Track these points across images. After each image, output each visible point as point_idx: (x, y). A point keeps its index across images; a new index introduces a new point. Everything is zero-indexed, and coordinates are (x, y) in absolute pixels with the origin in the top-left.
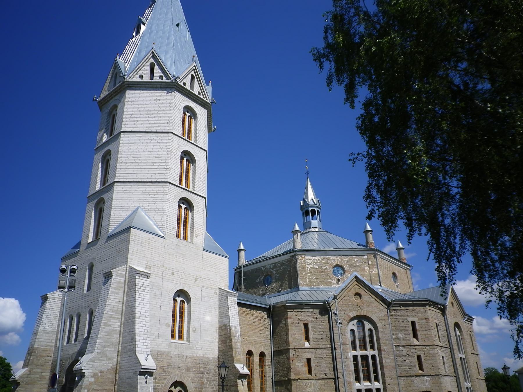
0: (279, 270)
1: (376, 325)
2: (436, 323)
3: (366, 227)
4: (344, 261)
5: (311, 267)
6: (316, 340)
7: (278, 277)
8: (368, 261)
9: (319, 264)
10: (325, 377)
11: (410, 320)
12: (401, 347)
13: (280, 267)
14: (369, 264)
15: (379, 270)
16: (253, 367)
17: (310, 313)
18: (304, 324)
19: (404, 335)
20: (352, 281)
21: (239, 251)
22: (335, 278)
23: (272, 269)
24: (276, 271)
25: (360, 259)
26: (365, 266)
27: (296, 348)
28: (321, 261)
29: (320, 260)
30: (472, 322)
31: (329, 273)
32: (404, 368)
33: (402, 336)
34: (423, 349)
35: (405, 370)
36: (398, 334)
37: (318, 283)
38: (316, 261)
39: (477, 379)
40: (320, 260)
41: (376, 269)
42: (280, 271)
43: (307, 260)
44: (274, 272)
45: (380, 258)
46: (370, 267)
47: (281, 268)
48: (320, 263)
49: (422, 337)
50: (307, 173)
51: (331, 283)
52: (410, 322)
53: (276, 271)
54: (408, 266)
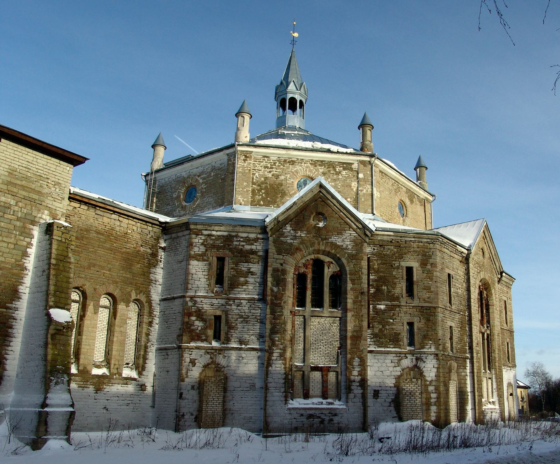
0: (208, 177)
2: (449, 275)
5: (259, 175)
7: (205, 188)
8: (358, 174)
14: (358, 178)
15: (375, 189)
16: (115, 322)
24: (203, 179)
26: (352, 181)
29: (277, 164)
31: (289, 187)
33: (387, 289)
38: (269, 166)
41: (369, 187)
42: (210, 178)
43: (254, 163)
44: (201, 181)
46: (360, 182)
47: (212, 175)
52: (405, 268)
53: (203, 179)
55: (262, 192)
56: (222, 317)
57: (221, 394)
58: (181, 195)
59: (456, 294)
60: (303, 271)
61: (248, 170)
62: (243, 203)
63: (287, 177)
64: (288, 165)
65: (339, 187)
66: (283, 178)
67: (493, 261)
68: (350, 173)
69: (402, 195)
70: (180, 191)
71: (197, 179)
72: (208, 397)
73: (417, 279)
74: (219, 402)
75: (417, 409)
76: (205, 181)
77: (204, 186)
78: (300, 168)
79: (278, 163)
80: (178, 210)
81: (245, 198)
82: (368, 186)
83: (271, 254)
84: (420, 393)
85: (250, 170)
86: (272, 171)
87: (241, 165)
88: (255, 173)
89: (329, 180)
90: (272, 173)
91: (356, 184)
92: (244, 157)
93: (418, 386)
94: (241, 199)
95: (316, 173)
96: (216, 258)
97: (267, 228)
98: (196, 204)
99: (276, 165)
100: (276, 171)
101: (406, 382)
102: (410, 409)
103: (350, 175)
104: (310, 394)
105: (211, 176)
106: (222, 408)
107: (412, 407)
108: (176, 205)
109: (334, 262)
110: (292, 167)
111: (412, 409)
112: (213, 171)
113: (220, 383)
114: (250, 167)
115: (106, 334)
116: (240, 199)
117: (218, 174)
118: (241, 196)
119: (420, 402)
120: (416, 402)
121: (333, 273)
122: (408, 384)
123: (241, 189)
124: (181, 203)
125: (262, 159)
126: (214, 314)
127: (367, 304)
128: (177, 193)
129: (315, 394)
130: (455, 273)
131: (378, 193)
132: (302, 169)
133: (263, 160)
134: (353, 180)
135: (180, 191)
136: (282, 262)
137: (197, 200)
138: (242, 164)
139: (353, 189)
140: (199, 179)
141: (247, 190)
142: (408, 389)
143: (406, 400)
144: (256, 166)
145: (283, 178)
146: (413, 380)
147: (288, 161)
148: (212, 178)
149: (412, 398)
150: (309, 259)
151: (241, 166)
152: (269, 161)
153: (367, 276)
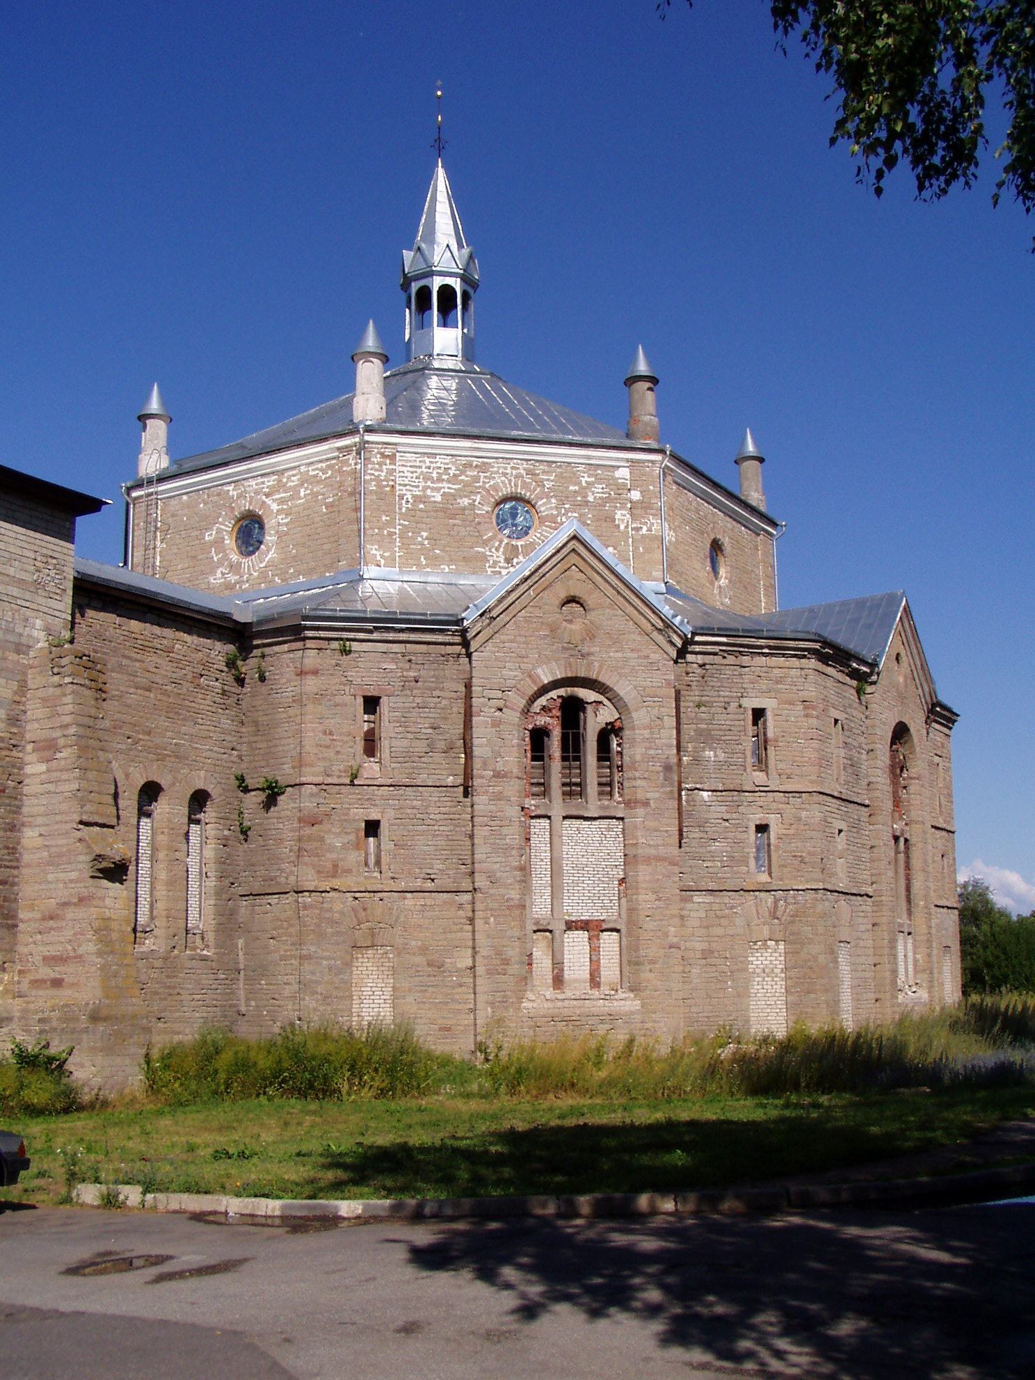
0: (292, 498)
1: (558, 680)
3: (633, 359)
4: (540, 484)
5: (414, 496)
6: (407, 757)
7: (286, 524)
9: (445, 485)
10: (429, 885)
11: (758, 704)
12: (705, 794)
13: (296, 489)
17: (393, 661)
18: (364, 697)
19: (722, 756)
20: (558, 551)
21: (143, 418)
22: (501, 542)
23: (267, 495)
24: (281, 501)
25: (599, 480)
27: (330, 780)
28: (454, 475)
30: (950, 728)
31: (479, 523)
32: (709, 864)
33: (716, 756)
34: (781, 806)
35: (710, 870)
36: (704, 750)
37: (437, 557)
38: (435, 475)
39: (936, 906)
40: (452, 472)
44: (275, 507)
45: (676, 482)
47: (302, 494)
48: (448, 481)
49: (781, 766)
50: (439, 147)
51: (484, 558)
52: (750, 712)
53: (281, 501)
54: (768, 525)
55: (422, 537)
56: (381, 823)
57: (388, 981)
58: (226, 537)
59: (849, 762)
60: (543, 723)
61: (388, 486)
62: (383, 562)
63: (475, 501)
64: (476, 473)
65: (589, 522)
66: (466, 503)
67: (916, 679)
68: (612, 490)
69: (716, 531)
70: (223, 527)
71: (264, 502)
72: (362, 989)
73: (775, 733)
74: (385, 997)
75: (778, 1002)
76: (285, 507)
77: (282, 519)
78: (503, 479)
79: (454, 468)
80: (219, 571)
81: (387, 552)
82: (651, 517)
83: (476, 688)
84: (782, 969)
85: (393, 486)
86: (441, 488)
87: (373, 474)
88: (404, 492)
89: (567, 506)
90: (443, 490)
91: (625, 516)
92: (379, 456)
93: (778, 954)
94: (378, 553)
95: (539, 489)
96: (362, 699)
97: (467, 632)
98: (267, 559)
99: (449, 474)
100: (448, 488)
101: (756, 947)
102: (764, 1003)
103: (612, 493)
104: (565, 976)
105: (300, 498)
106: (392, 1009)
107: (766, 999)
108: (215, 559)
109: (606, 702)
110: (485, 477)
111: (768, 1003)
112: (303, 485)
113: (384, 960)
114: (393, 480)
115: (618, 949)
116: (374, 552)
117: (318, 493)
118: (377, 547)
119: (783, 987)
120: (774, 987)
121: (604, 726)
122: (760, 951)
123: (377, 531)
124: (226, 557)
125: (418, 460)
126: (366, 819)
127: (676, 789)
128: (214, 533)
129: (575, 976)
130: (846, 716)
131: (672, 533)
132: (507, 482)
133: (420, 462)
134: (618, 505)
135: (223, 527)
136: (501, 703)
137: (268, 551)
138: (376, 473)
139: (618, 526)
140: (269, 501)
141: (388, 532)
142: (759, 962)
143: (756, 983)
144: (406, 477)
145: (466, 503)
146: (769, 942)
147: (475, 464)
148: (302, 501)
149: (766, 979)
150: (555, 698)
151: (373, 477)
152: (435, 465)
153: (674, 732)
